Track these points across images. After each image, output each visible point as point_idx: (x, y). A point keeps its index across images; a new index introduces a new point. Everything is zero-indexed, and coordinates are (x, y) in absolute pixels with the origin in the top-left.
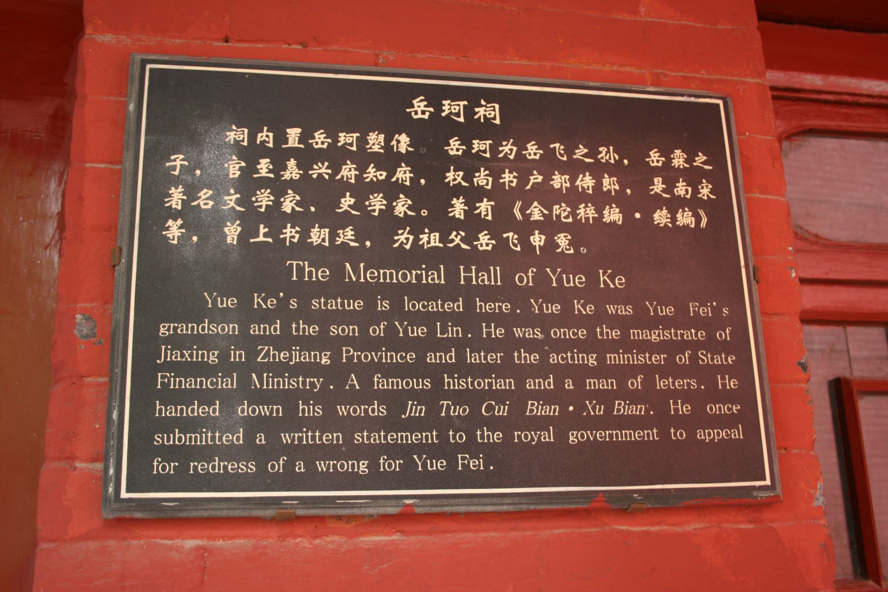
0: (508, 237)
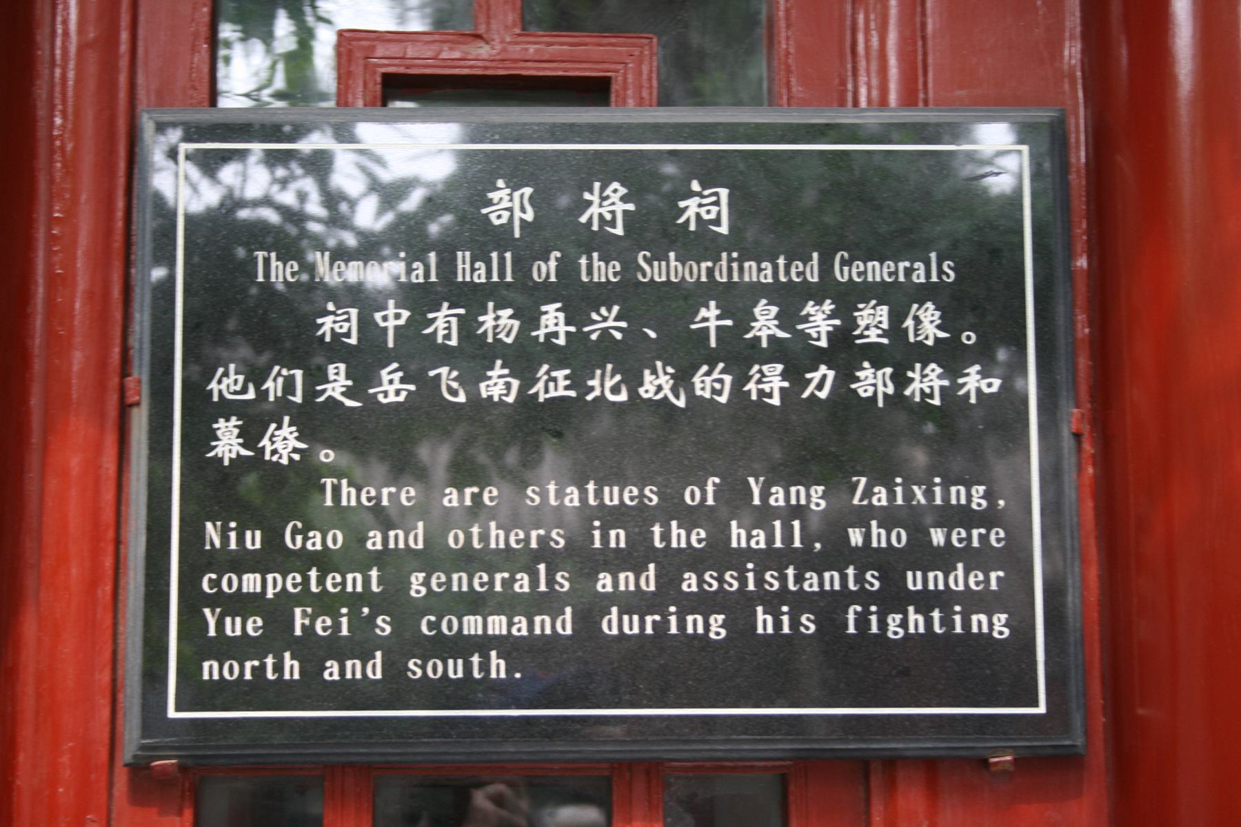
0: (439, 376)
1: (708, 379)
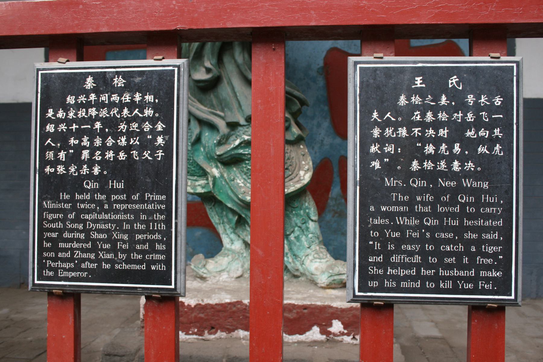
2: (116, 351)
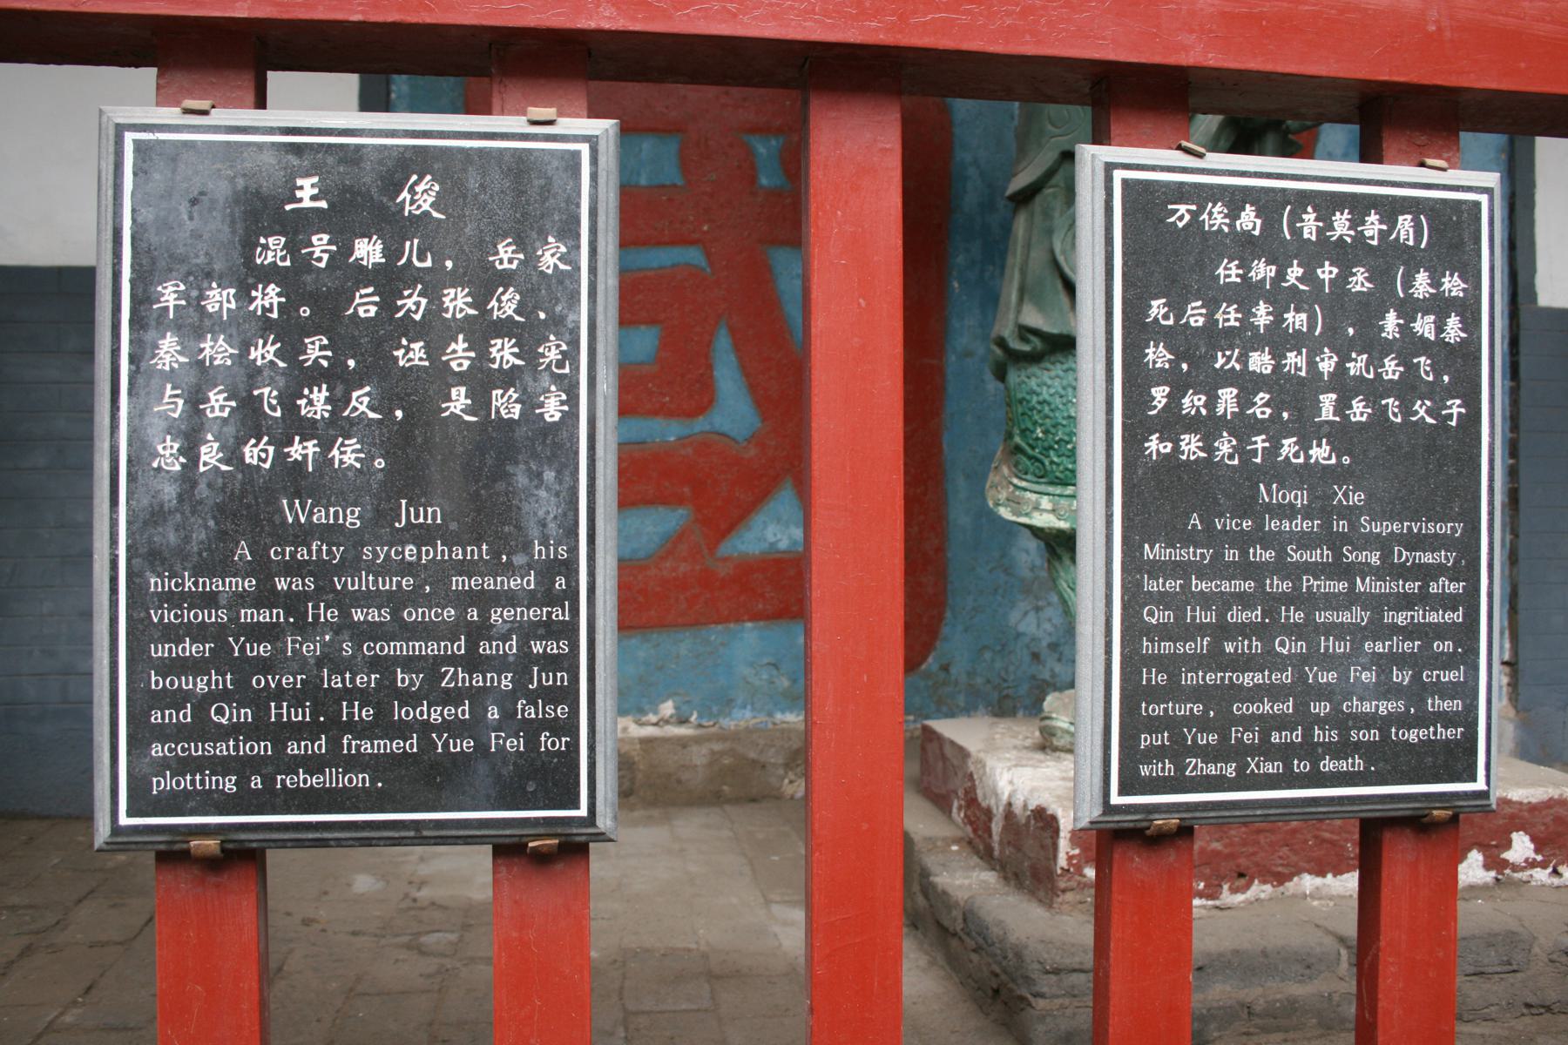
1: (256, 450)
2: (1077, 959)
